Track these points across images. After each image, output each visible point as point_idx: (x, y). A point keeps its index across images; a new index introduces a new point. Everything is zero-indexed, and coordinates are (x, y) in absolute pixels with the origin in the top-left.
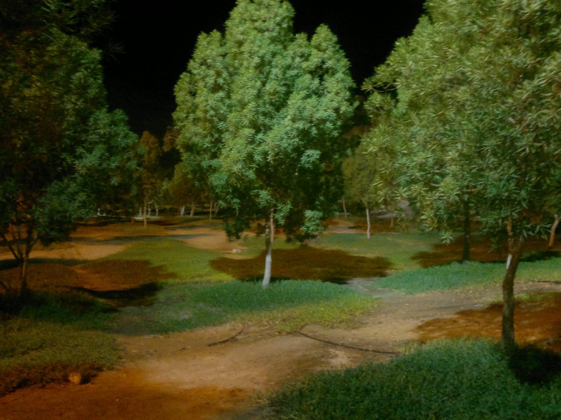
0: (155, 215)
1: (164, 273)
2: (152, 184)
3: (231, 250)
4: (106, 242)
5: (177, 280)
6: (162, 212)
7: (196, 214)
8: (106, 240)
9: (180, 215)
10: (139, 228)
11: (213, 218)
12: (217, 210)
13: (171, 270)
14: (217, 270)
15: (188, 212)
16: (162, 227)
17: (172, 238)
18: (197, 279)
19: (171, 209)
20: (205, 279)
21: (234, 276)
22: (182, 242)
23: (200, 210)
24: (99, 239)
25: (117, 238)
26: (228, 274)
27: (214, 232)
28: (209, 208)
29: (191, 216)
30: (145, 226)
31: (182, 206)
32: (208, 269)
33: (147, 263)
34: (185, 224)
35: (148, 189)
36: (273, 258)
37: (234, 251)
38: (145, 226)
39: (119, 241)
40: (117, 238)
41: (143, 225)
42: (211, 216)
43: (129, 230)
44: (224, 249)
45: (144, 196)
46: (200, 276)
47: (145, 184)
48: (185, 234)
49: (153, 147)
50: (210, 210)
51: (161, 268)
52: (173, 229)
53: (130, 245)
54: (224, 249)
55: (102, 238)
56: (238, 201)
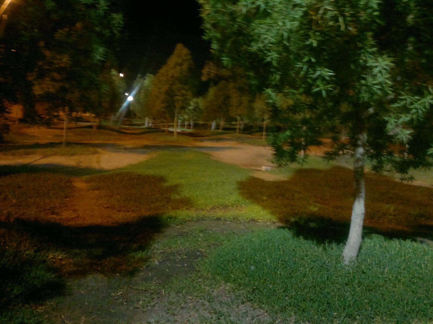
0: (190, 128)
1: (177, 197)
2: (183, 95)
3: (261, 166)
4: (133, 150)
5: (192, 213)
6: (196, 126)
7: (224, 129)
8: (135, 148)
9: (211, 129)
10: (169, 138)
11: (240, 133)
12: (242, 127)
13: (186, 193)
14: (247, 198)
15: (218, 127)
16: (192, 138)
17: (197, 150)
18: (220, 213)
19: (203, 125)
20: (231, 213)
21: (272, 213)
22: (207, 154)
23: (228, 126)
24: (127, 146)
25: (146, 147)
26: (264, 207)
27: (240, 146)
28: (236, 125)
29: (220, 131)
30: (175, 137)
31: (213, 121)
32: (235, 197)
33: (162, 179)
34: (214, 137)
35: (178, 100)
36: (367, 206)
37: (264, 168)
38: (175, 137)
39: (145, 150)
40: (146, 147)
41: (173, 135)
42: (237, 131)
43: (160, 139)
44: (251, 165)
45: (175, 107)
46: (225, 207)
47: (177, 95)
48: (213, 146)
49: (185, 58)
50: (237, 127)
51: (174, 188)
52: (202, 141)
53: (154, 155)
54: (251, 165)
55: (130, 146)
56: (328, 73)
